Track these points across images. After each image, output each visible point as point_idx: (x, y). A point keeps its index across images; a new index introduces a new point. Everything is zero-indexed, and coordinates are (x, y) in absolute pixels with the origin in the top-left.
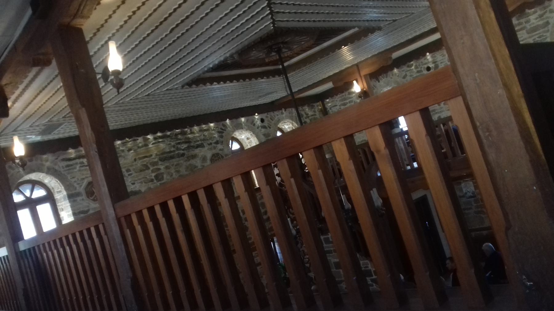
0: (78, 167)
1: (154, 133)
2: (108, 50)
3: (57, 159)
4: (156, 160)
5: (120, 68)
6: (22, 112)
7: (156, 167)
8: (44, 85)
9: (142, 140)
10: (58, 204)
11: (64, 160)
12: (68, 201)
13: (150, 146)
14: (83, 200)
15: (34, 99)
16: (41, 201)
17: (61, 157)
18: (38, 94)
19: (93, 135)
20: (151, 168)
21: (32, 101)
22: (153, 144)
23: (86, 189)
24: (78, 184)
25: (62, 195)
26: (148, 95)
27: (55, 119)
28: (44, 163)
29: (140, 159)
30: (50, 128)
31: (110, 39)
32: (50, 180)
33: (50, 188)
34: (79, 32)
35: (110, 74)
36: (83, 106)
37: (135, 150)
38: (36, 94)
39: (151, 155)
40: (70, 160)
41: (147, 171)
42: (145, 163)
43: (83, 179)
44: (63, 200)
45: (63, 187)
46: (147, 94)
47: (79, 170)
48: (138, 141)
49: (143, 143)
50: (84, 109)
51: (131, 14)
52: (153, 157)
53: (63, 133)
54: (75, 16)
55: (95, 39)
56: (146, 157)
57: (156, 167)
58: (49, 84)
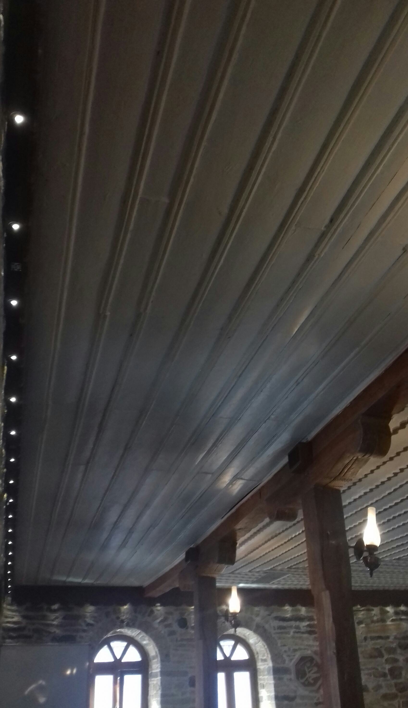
0: (292, 631)
1: (396, 604)
2: (366, 515)
3: (269, 615)
4: (394, 645)
5: (377, 542)
6: (246, 556)
7: (392, 656)
8: (278, 532)
9: (379, 612)
10: (260, 677)
11: (276, 618)
12: (272, 677)
13: (389, 623)
14: (291, 680)
15: (263, 544)
16: (133, 668)
17: (274, 615)
18: (269, 540)
19: (334, 628)
20: (386, 657)
21: (260, 546)
22: (393, 620)
23: (297, 664)
24: (289, 656)
25: (266, 667)
26: (399, 559)
27: (279, 568)
28: (254, 617)
29: (372, 638)
30: (270, 576)
31: (371, 505)
32: (257, 641)
33: (255, 652)
34: (337, 495)
35: (365, 549)
36: (328, 588)
37: (367, 625)
38: (267, 539)
39: (388, 637)
40: (284, 619)
41: (379, 659)
42: (379, 647)
43: (295, 650)
44: (266, 673)
45: (269, 656)
46: (397, 557)
47: (293, 637)
48: (373, 612)
49: (379, 617)
50: (327, 592)
51: (398, 471)
52: (391, 639)
53: (283, 585)
54: (335, 479)
55: (347, 493)
56: (380, 637)
57: (392, 656)
58: (283, 531)
